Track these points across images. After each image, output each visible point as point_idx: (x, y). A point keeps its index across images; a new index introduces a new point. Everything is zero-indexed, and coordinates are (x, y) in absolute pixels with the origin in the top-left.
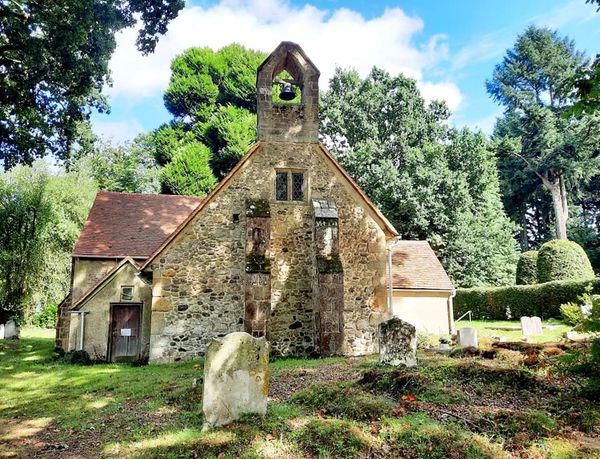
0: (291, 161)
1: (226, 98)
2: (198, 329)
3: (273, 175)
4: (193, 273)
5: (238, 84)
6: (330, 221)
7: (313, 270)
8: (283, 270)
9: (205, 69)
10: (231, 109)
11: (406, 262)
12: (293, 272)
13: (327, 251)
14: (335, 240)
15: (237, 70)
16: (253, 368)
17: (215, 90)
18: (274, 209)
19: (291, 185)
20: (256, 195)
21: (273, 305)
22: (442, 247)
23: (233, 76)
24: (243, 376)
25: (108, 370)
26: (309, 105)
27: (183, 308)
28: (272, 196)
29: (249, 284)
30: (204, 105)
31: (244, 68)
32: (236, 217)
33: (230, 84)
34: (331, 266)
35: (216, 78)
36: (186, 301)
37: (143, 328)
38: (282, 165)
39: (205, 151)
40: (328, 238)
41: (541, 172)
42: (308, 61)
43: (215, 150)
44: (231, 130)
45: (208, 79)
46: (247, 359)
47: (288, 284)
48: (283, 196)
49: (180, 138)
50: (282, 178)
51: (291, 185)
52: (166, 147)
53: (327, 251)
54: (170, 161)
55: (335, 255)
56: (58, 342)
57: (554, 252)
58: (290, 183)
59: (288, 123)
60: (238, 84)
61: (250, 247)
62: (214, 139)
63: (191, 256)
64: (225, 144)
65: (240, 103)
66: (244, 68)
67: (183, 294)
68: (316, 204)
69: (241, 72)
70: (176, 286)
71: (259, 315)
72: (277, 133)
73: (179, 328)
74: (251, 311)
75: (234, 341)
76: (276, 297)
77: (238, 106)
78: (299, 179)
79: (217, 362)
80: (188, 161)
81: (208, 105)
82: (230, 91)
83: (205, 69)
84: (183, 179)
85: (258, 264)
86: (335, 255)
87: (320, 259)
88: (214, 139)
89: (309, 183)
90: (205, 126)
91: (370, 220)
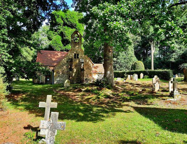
0: (76, 52)
1: (65, 24)
2: (61, 79)
3: (74, 54)
4: (60, 70)
5: (68, 21)
6: (83, 63)
7: (80, 70)
8: (75, 70)
9: (60, 17)
10: (66, 27)
11: (98, 68)
12: (76, 71)
13: (82, 67)
14: (83, 66)
15: (68, 17)
16: (69, 83)
17: (62, 22)
18: (73, 60)
19: (76, 56)
20: (70, 58)
21: (73, 76)
22: (115, 61)
23: (67, 19)
24: (68, 83)
25: (46, 85)
26: (80, 42)
27: (59, 76)
28: (73, 58)
29: (69, 72)
30: (60, 26)
31: (69, 17)
32: (67, 61)
33: (66, 21)
34: (83, 70)
35: (62, 19)
36: (59, 75)
37: (51, 79)
38: (75, 53)
39: (60, 37)
40: (82, 65)
41: (149, 39)
42: (80, 34)
43: (62, 37)
44: (66, 33)
45: (60, 19)
46: (68, 82)
47: (76, 72)
48: (75, 58)
49: (54, 34)
50: (75, 55)
51: (76, 56)
52: (50, 36)
53: (82, 67)
54: (52, 40)
55: (83, 68)
56: (33, 81)
57: (136, 64)
58: (76, 55)
59: (76, 45)
60: (68, 21)
61: (70, 67)
62: (62, 34)
63: (60, 68)
64: (65, 36)
65: (68, 26)
66: (69, 17)
67: (59, 74)
68: (81, 59)
69: (69, 18)
70: (58, 72)
71: (71, 77)
72: (74, 47)
73: (58, 79)
74: (70, 77)
75: (67, 81)
76: (74, 74)
77: (68, 27)
78: (78, 55)
79: (65, 82)
80: (56, 40)
81: (61, 26)
82: (66, 23)
83: (60, 17)
84: (55, 45)
85: (71, 69)
86: (83, 68)
87: (81, 69)
88: (62, 34)
89: (79, 56)
90: (60, 31)
91: (90, 62)
